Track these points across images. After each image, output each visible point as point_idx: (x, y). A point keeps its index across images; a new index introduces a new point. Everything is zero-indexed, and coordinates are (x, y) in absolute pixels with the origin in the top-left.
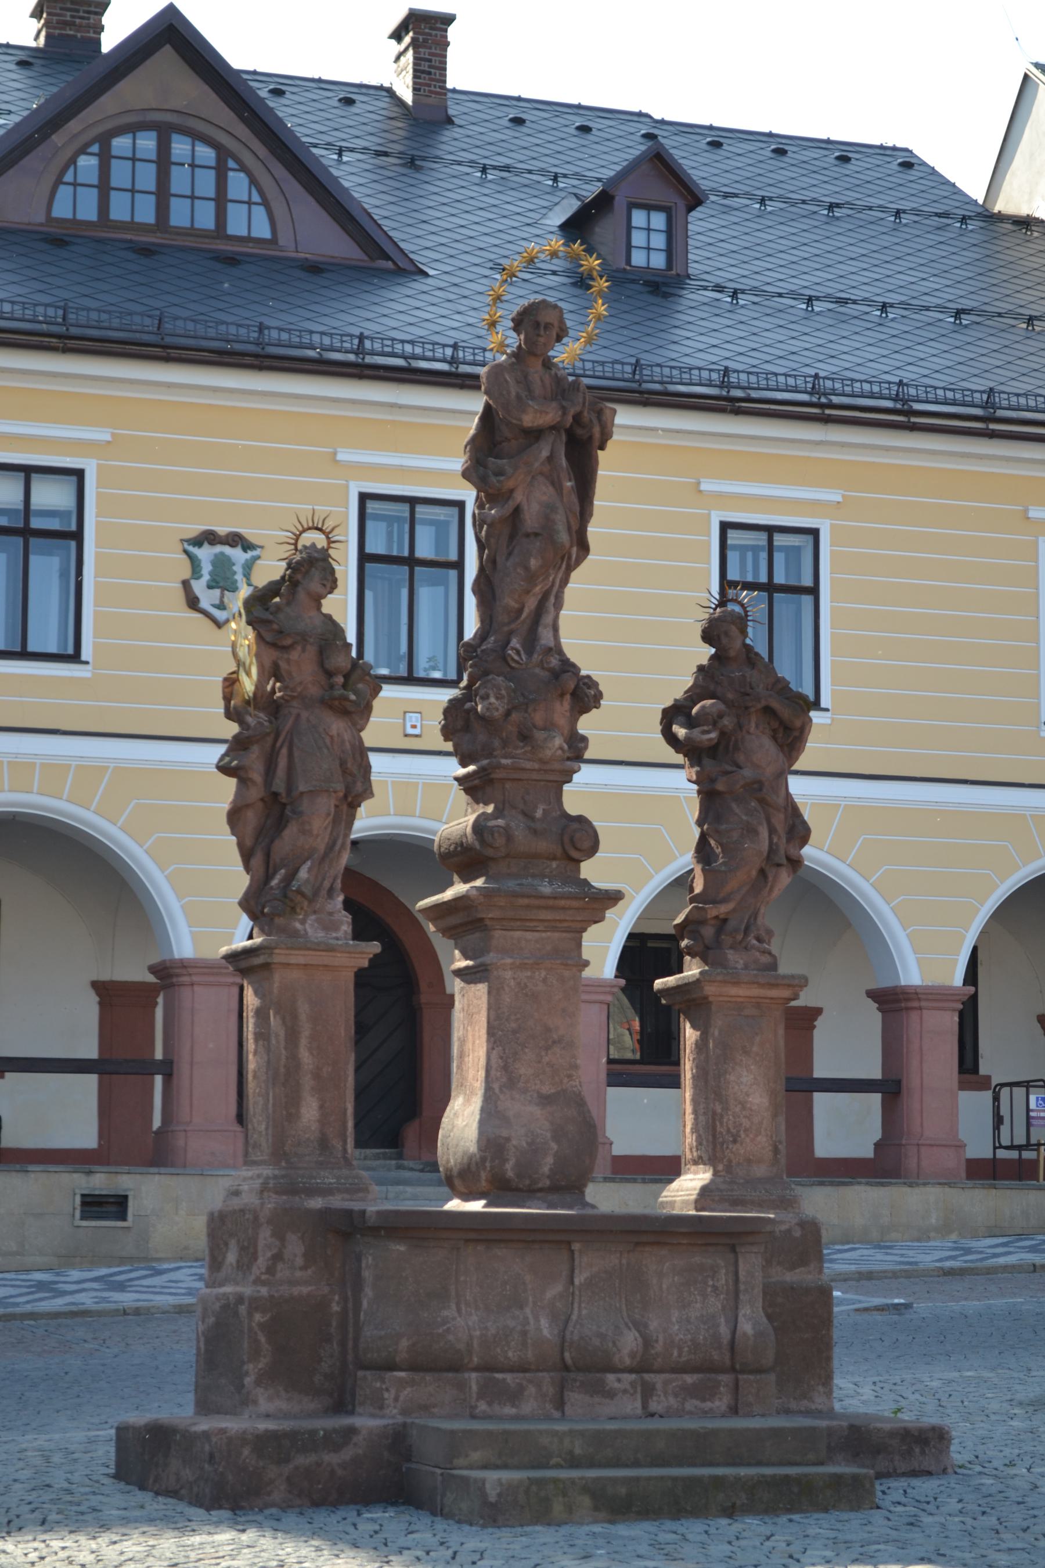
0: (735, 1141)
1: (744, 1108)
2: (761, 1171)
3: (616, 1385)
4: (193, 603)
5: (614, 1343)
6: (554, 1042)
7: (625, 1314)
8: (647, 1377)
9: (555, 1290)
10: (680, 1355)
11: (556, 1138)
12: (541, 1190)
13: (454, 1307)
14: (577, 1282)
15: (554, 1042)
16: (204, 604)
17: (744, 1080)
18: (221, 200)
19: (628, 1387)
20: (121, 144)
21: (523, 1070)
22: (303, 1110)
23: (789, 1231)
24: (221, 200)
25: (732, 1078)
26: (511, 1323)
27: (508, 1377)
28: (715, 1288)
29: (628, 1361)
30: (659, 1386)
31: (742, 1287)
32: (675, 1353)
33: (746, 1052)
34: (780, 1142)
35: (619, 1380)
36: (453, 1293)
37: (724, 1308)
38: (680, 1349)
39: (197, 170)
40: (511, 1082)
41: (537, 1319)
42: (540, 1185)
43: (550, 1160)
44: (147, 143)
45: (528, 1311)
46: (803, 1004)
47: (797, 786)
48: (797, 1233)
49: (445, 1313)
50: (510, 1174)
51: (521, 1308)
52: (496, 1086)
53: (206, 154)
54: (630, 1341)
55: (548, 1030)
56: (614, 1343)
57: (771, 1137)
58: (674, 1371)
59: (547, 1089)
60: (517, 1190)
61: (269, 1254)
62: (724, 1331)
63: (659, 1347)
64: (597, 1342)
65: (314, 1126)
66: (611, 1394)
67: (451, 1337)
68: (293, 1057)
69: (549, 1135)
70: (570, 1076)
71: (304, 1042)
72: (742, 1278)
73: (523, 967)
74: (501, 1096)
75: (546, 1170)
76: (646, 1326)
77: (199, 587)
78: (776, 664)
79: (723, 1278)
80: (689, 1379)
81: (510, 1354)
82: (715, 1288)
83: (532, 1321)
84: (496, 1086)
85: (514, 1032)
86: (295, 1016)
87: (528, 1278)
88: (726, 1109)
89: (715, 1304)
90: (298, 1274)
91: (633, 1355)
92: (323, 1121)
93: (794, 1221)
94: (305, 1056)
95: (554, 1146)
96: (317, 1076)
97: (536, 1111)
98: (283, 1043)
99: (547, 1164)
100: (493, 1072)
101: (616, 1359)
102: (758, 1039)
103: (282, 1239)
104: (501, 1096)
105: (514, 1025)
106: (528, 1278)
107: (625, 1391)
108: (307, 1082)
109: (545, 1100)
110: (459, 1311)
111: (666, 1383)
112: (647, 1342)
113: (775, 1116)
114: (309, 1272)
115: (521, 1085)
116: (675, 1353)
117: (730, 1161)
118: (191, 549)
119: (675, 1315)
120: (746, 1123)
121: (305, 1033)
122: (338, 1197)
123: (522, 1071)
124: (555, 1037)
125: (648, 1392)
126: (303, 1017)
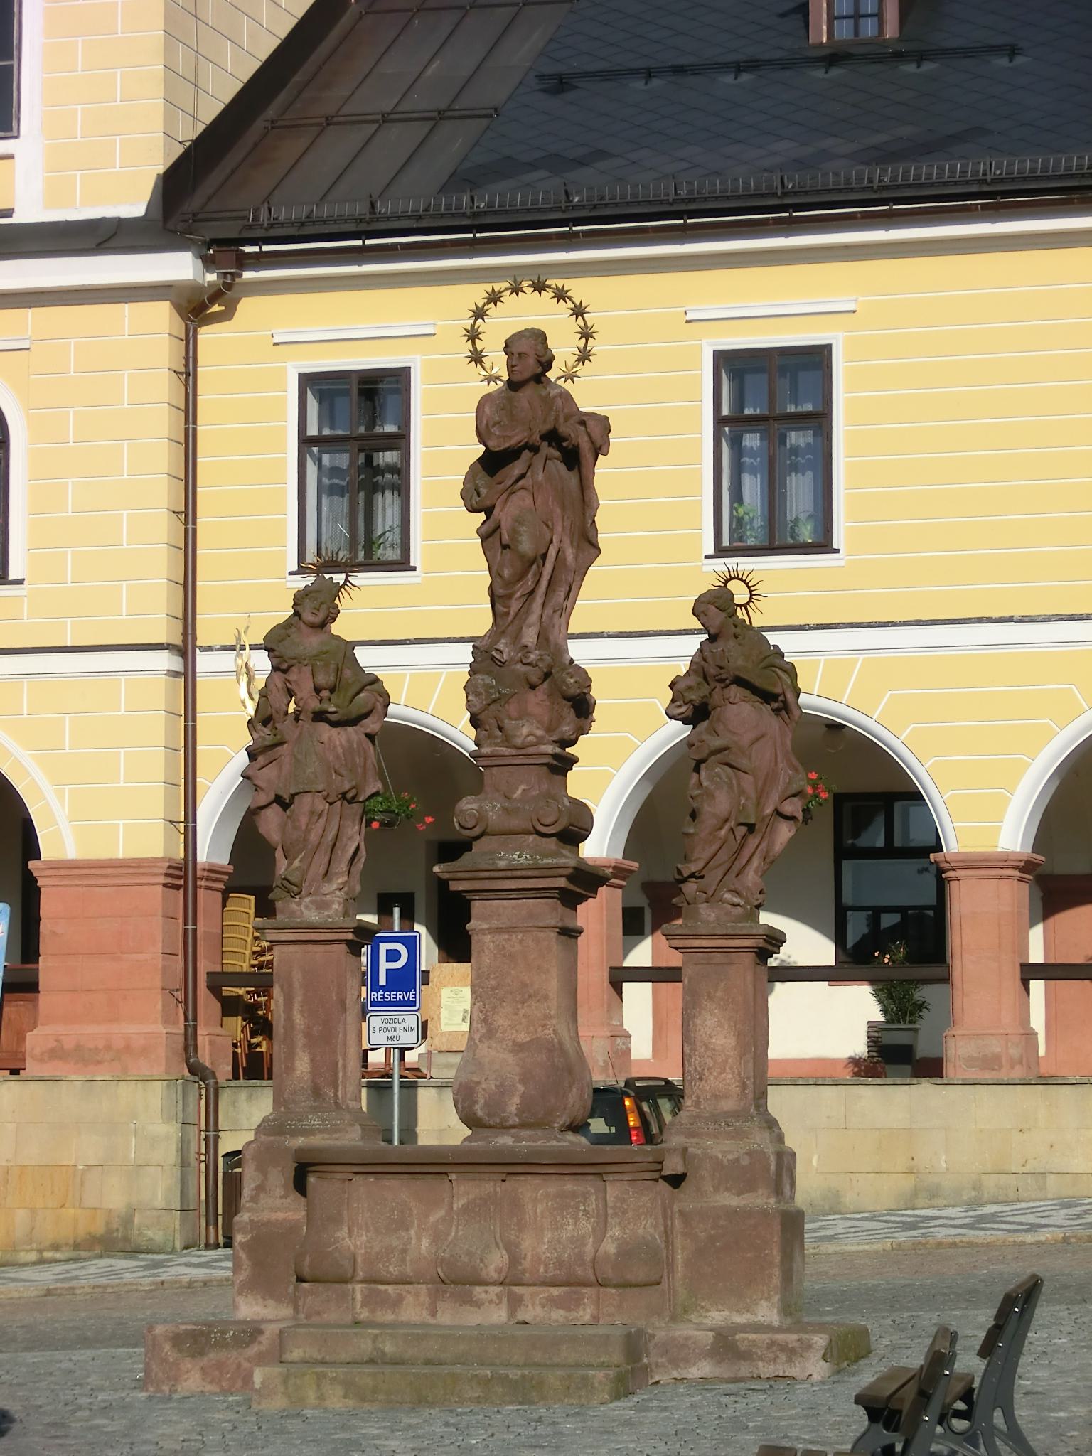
0: (701, 1079)
1: (707, 1048)
2: (728, 1105)
3: (483, 1296)
5: (482, 1261)
6: (530, 996)
7: (498, 1235)
8: (515, 1289)
10: (546, 1271)
11: (523, 1081)
12: (513, 1127)
13: (346, 1230)
15: (530, 996)
17: (708, 1023)
19: (494, 1298)
21: (500, 1021)
22: (297, 1064)
23: (737, 1160)
26: (395, 1243)
27: (390, 1288)
28: (586, 1212)
29: (495, 1276)
30: (527, 1298)
31: (610, 1211)
32: (542, 1269)
33: (710, 998)
34: (748, 1078)
35: (486, 1292)
36: (346, 1218)
37: (594, 1230)
38: (546, 1266)
40: (490, 1033)
41: (419, 1239)
42: (511, 1122)
43: (516, 1100)
45: (412, 1232)
47: (577, 651)
48: (745, 1161)
49: (338, 1234)
50: (480, 1113)
51: (407, 1230)
52: (477, 1037)
54: (496, 1261)
55: (524, 985)
56: (482, 1261)
57: (739, 1074)
58: (544, 1284)
59: (523, 1037)
60: (491, 1127)
61: (253, 1186)
62: (589, 1248)
63: (526, 1264)
64: (465, 1259)
66: (478, 1304)
67: (337, 1254)
69: (517, 1078)
70: (544, 1026)
71: (296, 1006)
72: (610, 1204)
73: (499, 930)
74: (480, 1046)
75: (513, 1109)
76: (518, 1245)
78: (179, 327)
79: (593, 1204)
80: (555, 1291)
81: (391, 1269)
82: (586, 1212)
83: (414, 1242)
84: (477, 1037)
85: (493, 989)
86: (291, 985)
87: (413, 1204)
88: (693, 1050)
89: (586, 1226)
90: (278, 1202)
91: (499, 1271)
92: (315, 1071)
93: (742, 1152)
94: (298, 1019)
95: (521, 1088)
96: (308, 1034)
97: (510, 1058)
98: (282, 1008)
99: (513, 1105)
100: (475, 1025)
101: (484, 1273)
102: (722, 985)
103: (265, 1174)
104: (480, 1046)
105: (493, 983)
106: (413, 1204)
107: (491, 1301)
108: (300, 1040)
109: (519, 1048)
111: (533, 1295)
112: (515, 1260)
113: (742, 1056)
114: (288, 1200)
115: (498, 1035)
116: (542, 1269)
117: (698, 1097)
119: (548, 1236)
120: (710, 1062)
122: (319, 1136)
123: (500, 1022)
124: (531, 991)
125: (515, 1303)
126: (296, 985)
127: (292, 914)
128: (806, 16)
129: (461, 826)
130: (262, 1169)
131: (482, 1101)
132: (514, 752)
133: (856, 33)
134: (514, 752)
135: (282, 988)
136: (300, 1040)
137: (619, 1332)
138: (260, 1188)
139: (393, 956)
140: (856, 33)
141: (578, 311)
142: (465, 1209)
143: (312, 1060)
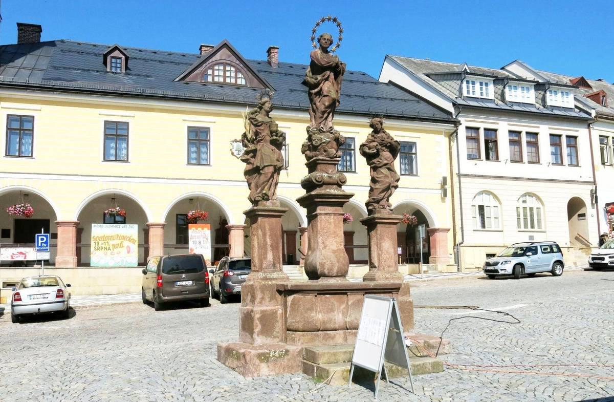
0: (385, 262)
4: (233, 154)
9: (343, 306)
11: (338, 262)
14: (349, 304)
16: (235, 154)
18: (236, 78)
20: (216, 67)
24: (236, 78)
25: (383, 244)
39: (462, 179)
43: (337, 268)
44: (221, 68)
46: (305, 124)
49: (312, 315)
53: (233, 69)
65: (272, 260)
68: (265, 240)
71: (268, 237)
77: (234, 151)
86: (265, 229)
92: (274, 259)
95: (337, 264)
96: (272, 246)
103: (264, 294)
110: (316, 314)
118: (232, 143)
121: (268, 234)
127: (265, 205)
128: (119, 122)
129: (317, 181)
130: (262, 292)
131: (326, 269)
132: (329, 159)
133: (117, 133)
134: (329, 159)
135: (262, 230)
136: (269, 248)
137: (238, 310)
138: (263, 298)
139: (42, 239)
140: (117, 133)
141: (339, 25)
142: (353, 304)
143: (273, 255)
